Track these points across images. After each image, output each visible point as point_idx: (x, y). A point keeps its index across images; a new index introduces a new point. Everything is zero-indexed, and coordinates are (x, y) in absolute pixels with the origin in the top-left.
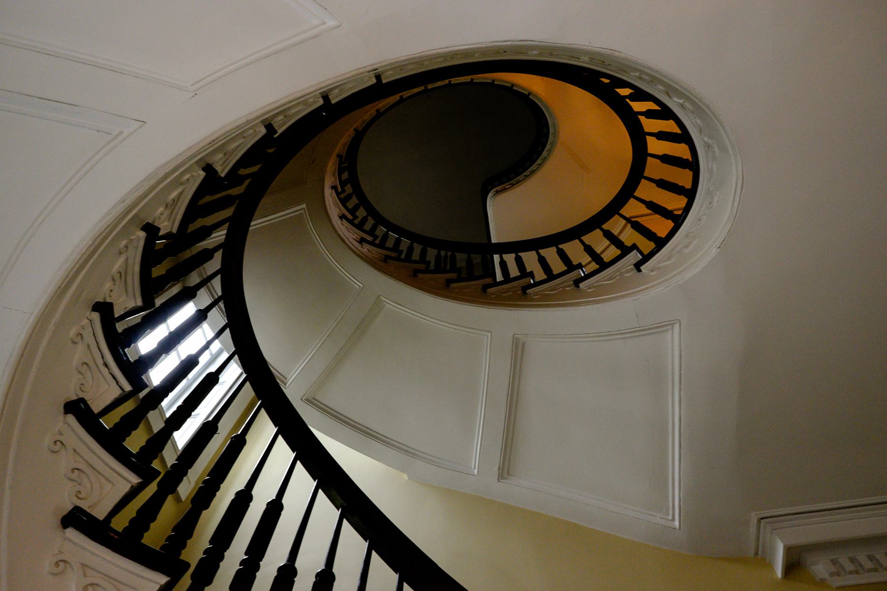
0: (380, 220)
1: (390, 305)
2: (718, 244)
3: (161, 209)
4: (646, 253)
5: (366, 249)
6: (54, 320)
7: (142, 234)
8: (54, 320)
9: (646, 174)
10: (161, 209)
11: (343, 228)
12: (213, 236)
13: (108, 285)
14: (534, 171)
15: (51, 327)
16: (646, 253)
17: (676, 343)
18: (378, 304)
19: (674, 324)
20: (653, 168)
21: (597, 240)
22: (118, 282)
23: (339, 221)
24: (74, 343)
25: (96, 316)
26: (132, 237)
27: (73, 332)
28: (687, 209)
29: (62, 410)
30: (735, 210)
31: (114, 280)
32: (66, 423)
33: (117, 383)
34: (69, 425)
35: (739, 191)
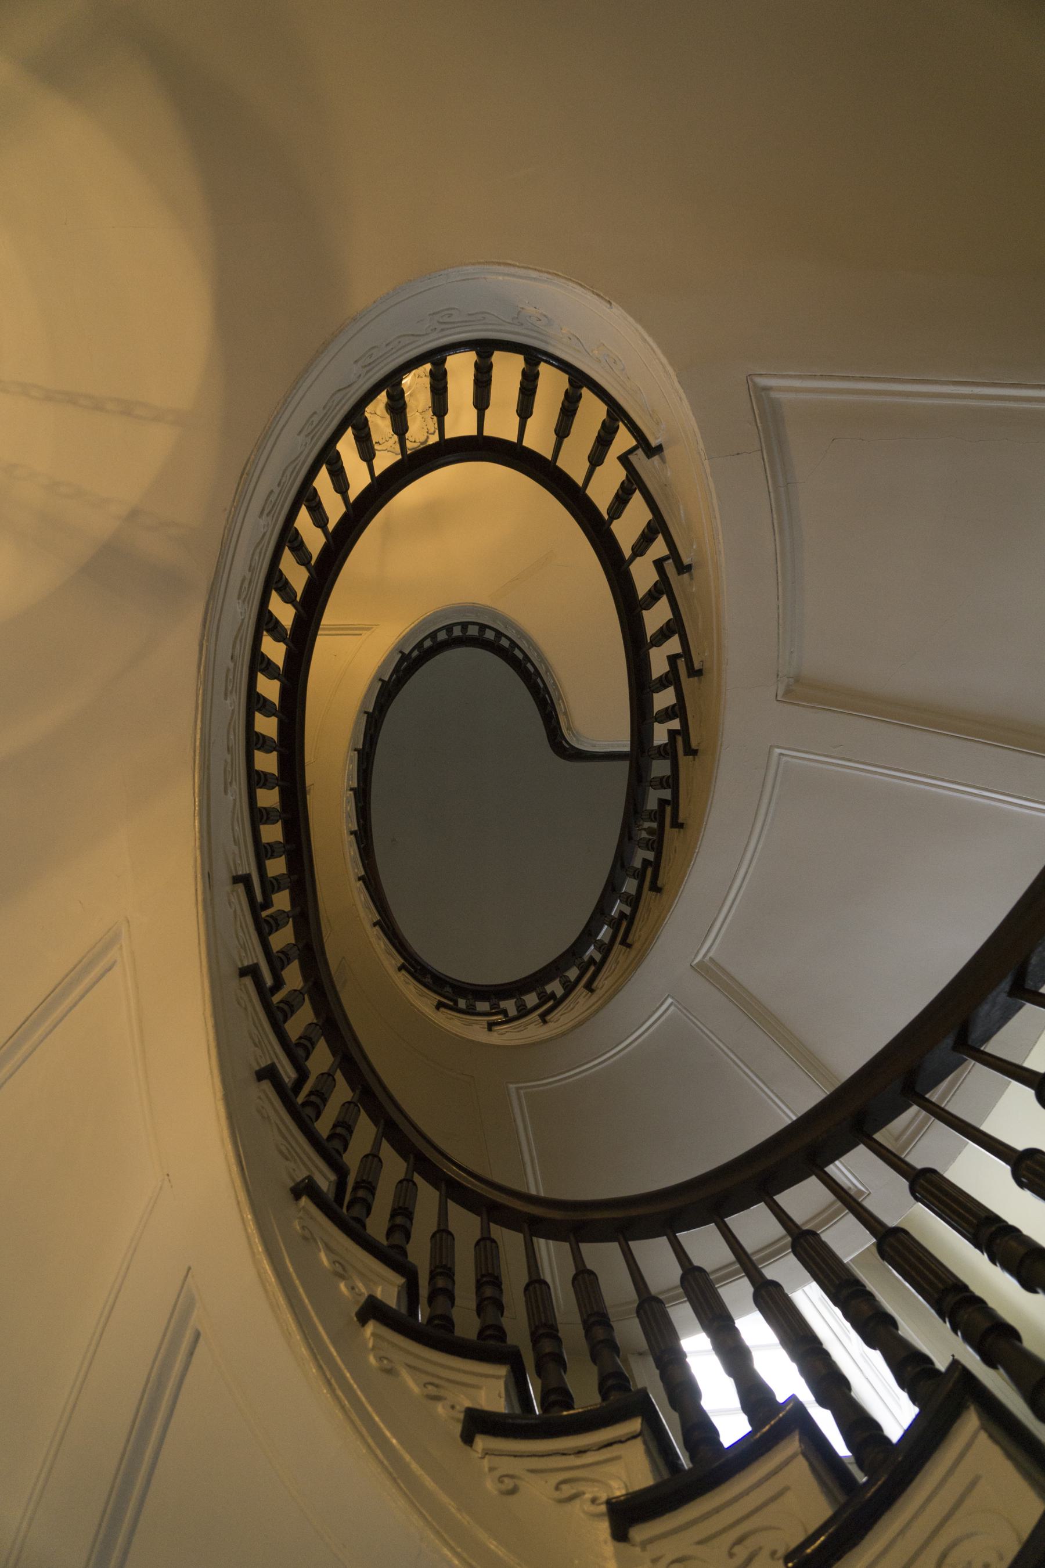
0: (574, 953)
1: (710, 948)
2: (604, 306)
3: (342, 1286)
4: (634, 443)
5: (604, 983)
6: (452, 1507)
7: (371, 1328)
8: (452, 1507)
9: (474, 432)
10: (342, 1286)
11: (563, 1019)
12: (549, 1280)
13: (440, 1409)
14: (539, 655)
15: (465, 1519)
16: (634, 443)
17: (797, 383)
18: (708, 971)
19: (755, 385)
20: (461, 422)
21: (627, 529)
22: (442, 1392)
23: (551, 1025)
24: (513, 1491)
25: (481, 1442)
26: (370, 1345)
27: (490, 1485)
28: (563, 366)
29: (468, 1448)
30: (545, 276)
31: (437, 1398)
32: (644, 1545)
33: (621, 1442)
34: (651, 1541)
35: (512, 270)
